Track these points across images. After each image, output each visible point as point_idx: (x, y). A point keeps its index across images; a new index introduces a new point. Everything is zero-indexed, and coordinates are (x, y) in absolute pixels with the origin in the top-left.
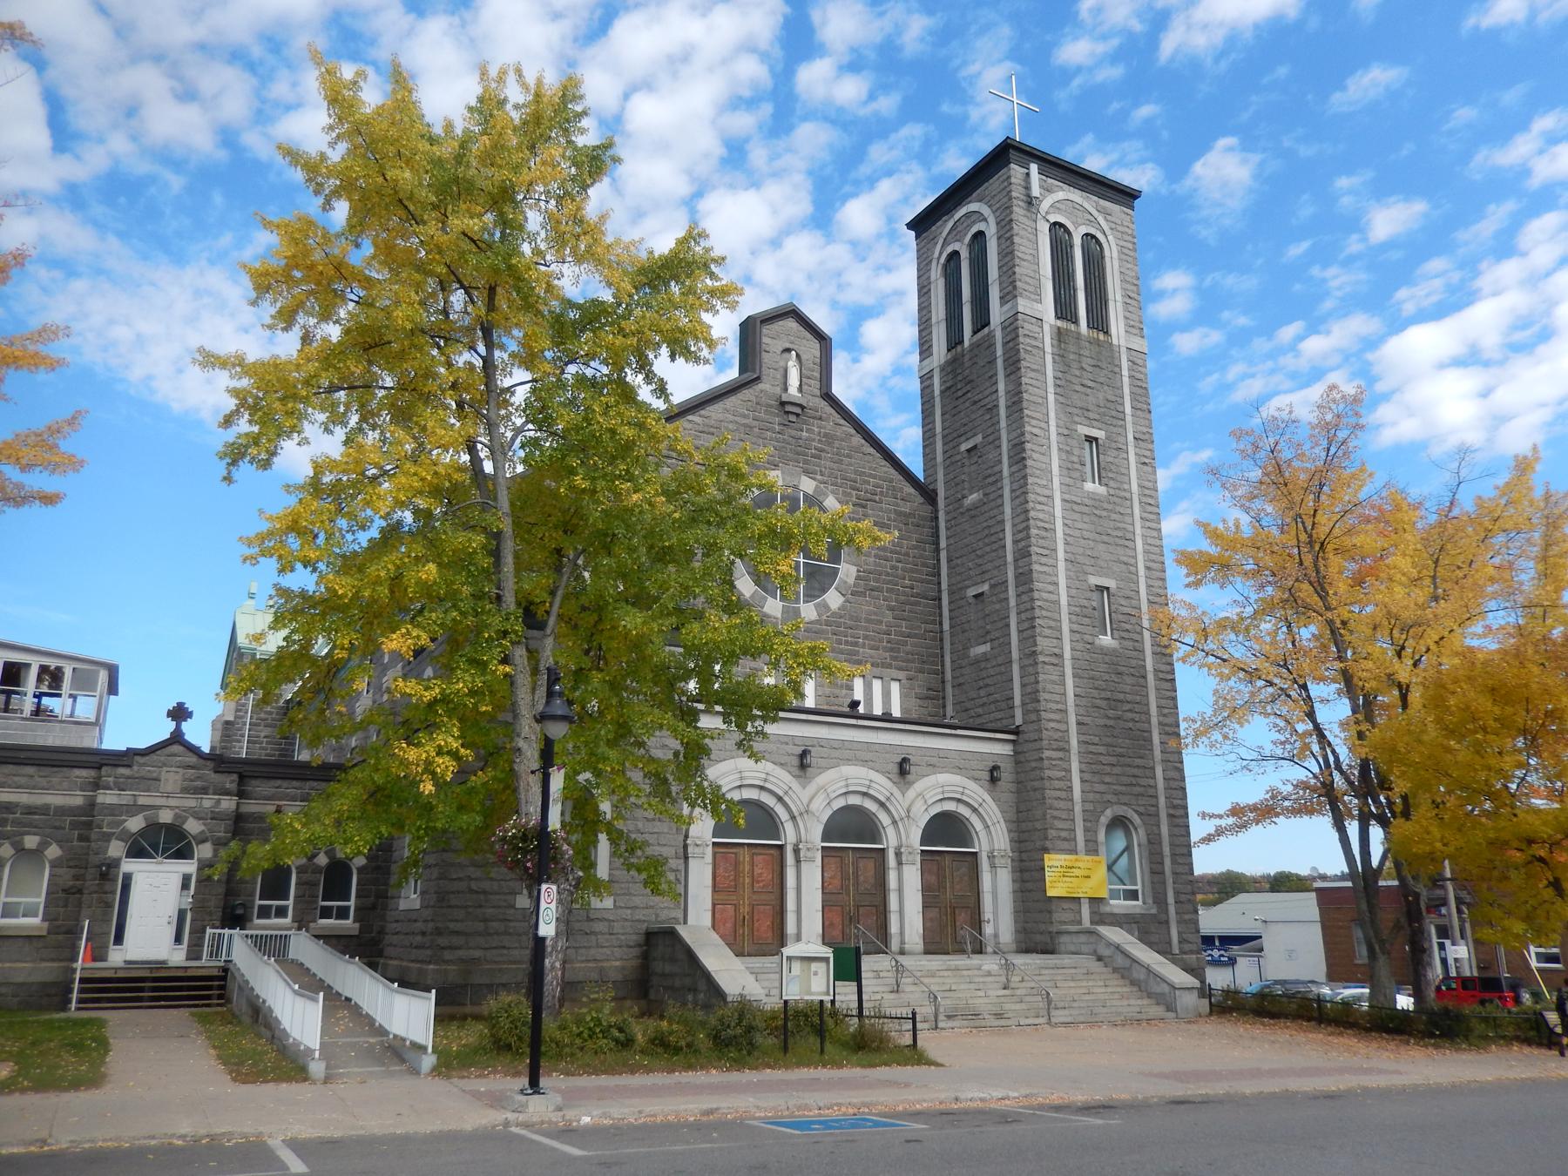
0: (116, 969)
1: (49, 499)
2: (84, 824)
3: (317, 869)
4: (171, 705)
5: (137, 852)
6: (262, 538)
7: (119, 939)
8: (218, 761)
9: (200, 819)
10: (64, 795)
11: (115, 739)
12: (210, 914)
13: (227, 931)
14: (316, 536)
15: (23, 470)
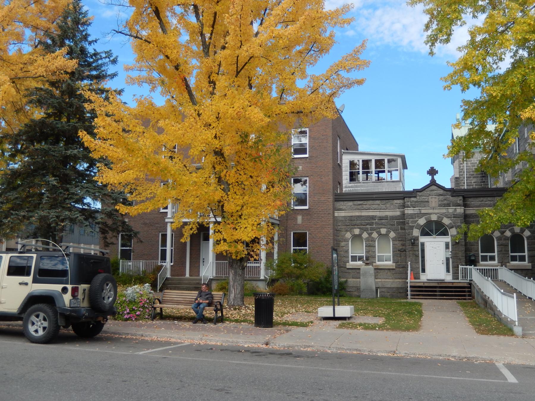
0: (424, 283)
1: (360, 82)
2: (402, 223)
3: (506, 238)
4: (428, 169)
5: (425, 233)
6: (451, 76)
7: (424, 271)
8: (453, 192)
9: (448, 218)
10: (392, 211)
11: (409, 188)
12: (460, 259)
13: (468, 267)
14: (477, 69)
15: (348, 71)
